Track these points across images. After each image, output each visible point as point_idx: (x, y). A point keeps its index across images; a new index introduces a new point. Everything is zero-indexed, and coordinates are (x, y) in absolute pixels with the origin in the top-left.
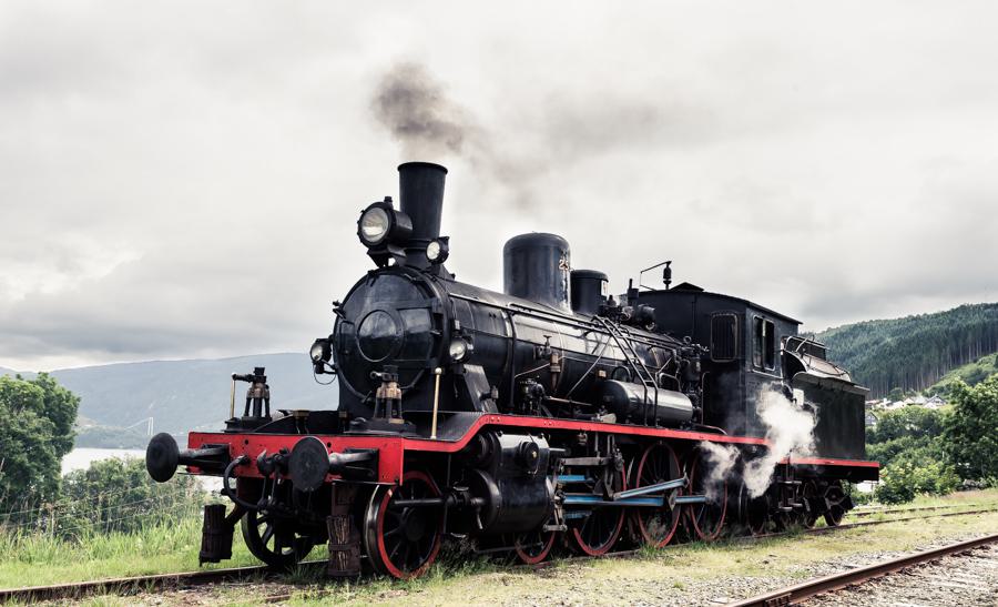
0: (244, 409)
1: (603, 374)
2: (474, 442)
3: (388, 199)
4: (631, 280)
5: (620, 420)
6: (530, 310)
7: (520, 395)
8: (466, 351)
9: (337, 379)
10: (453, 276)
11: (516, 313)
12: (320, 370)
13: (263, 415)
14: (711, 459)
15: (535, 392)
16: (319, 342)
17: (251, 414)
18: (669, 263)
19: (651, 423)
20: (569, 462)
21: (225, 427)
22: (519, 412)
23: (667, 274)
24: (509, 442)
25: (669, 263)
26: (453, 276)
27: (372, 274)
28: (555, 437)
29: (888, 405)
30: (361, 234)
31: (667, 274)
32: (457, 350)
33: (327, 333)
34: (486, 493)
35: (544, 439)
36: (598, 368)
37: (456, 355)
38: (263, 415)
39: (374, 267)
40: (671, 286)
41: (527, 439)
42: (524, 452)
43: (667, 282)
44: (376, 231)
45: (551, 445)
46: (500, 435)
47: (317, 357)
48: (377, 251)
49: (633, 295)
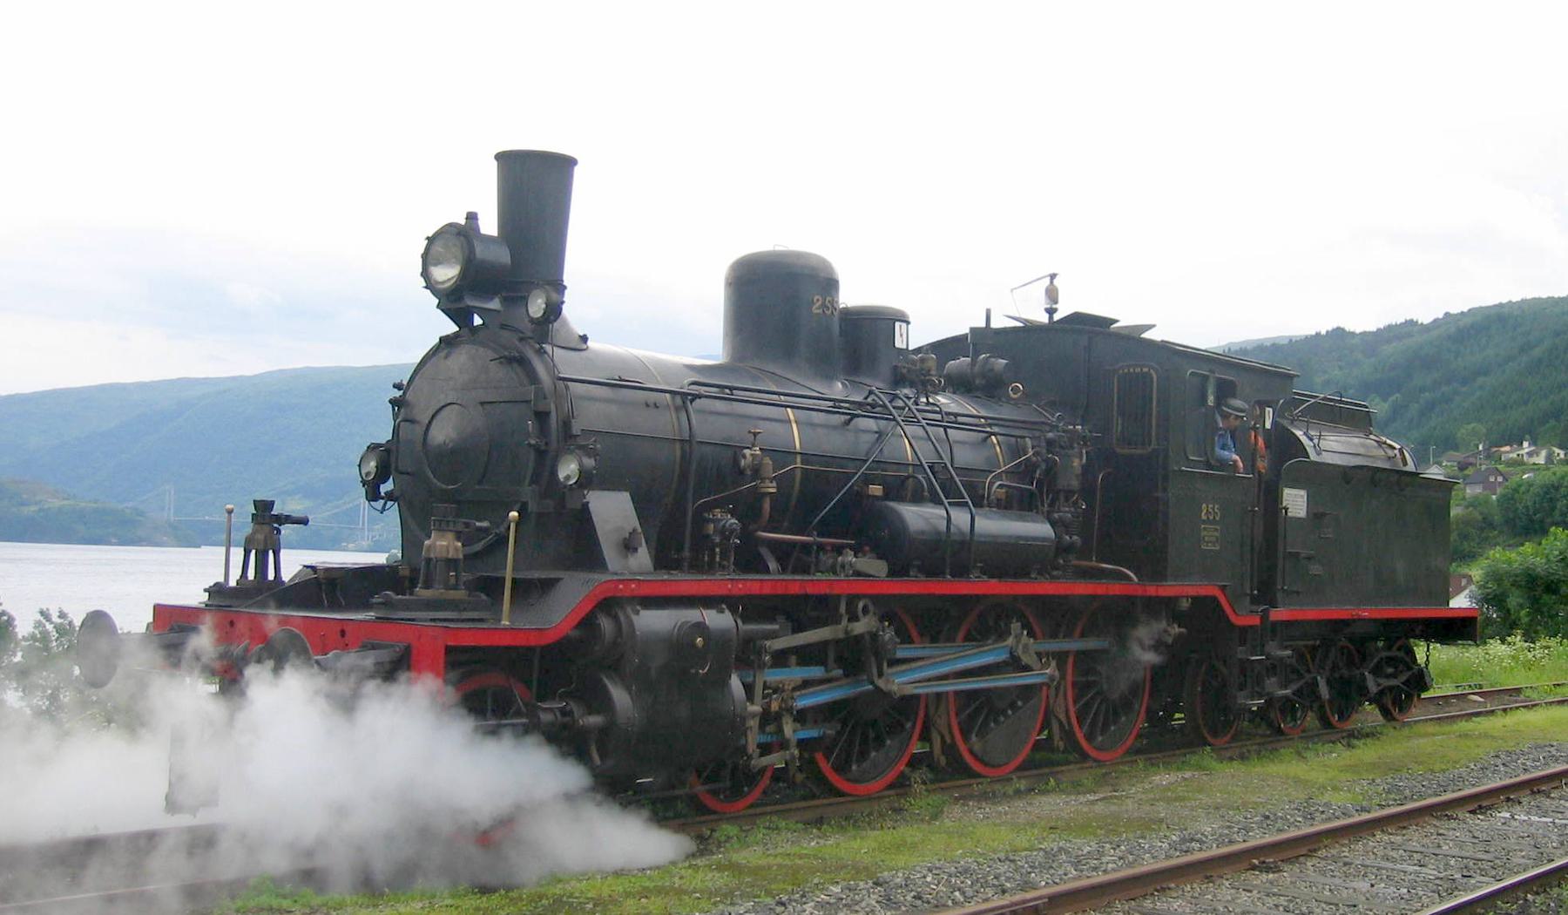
1: (876, 490)
2: (587, 623)
3: (472, 217)
4: (304, 521)
6: (732, 388)
7: (701, 542)
9: (396, 504)
10: (584, 339)
12: (373, 495)
13: (271, 576)
15: (725, 534)
16: (373, 448)
17: (251, 575)
18: (1053, 276)
19: (961, 571)
23: (1052, 295)
24: (654, 622)
25: (1053, 276)
26: (584, 339)
27: (446, 342)
30: (425, 274)
31: (1052, 295)
32: (568, 470)
33: (384, 435)
36: (868, 480)
37: (568, 478)
38: (271, 576)
39: (450, 328)
40: (1057, 317)
41: (692, 615)
42: (681, 647)
43: (1051, 312)
44: (447, 273)
45: (1385, 400)
47: (368, 474)
48: (452, 301)
49: (23, 637)
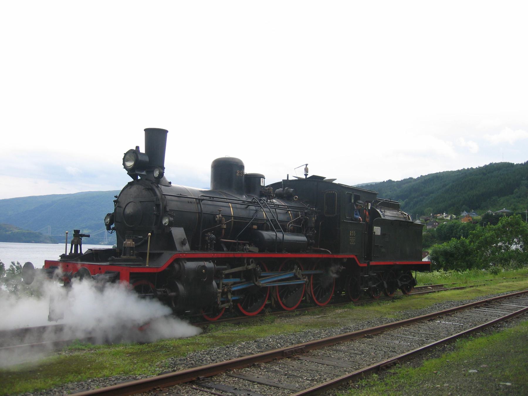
0: (65, 247)
1: (255, 227)
2: (171, 266)
3: (137, 148)
5: (261, 251)
8: (169, 221)
10: (170, 183)
11: (204, 200)
14: (478, 167)
16: (109, 215)
17: (73, 252)
18: (307, 165)
19: (280, 251)
20: (227, 272)
21: (60, 258)
22: (203, 249)
23: (306, 170)
24: (190, 265)
25: (307, 165)
26: (170, 183)
27: (130, 184)
28: (218, 261)
29: (446, 217)
31: (306, 170)
32: (166, 221)
33: (112, 211)
34: (176, 289)
35: (212, 263)
36: (253, 224)
37: (165, 223)
38: (79, 252)
39: (131, 180)
40: (308, 177)
41: (202, 263)
42: (198, 272)
43: (306, 175)
44: (130, 164)
46: (186, 263)
47: (107, 222)
